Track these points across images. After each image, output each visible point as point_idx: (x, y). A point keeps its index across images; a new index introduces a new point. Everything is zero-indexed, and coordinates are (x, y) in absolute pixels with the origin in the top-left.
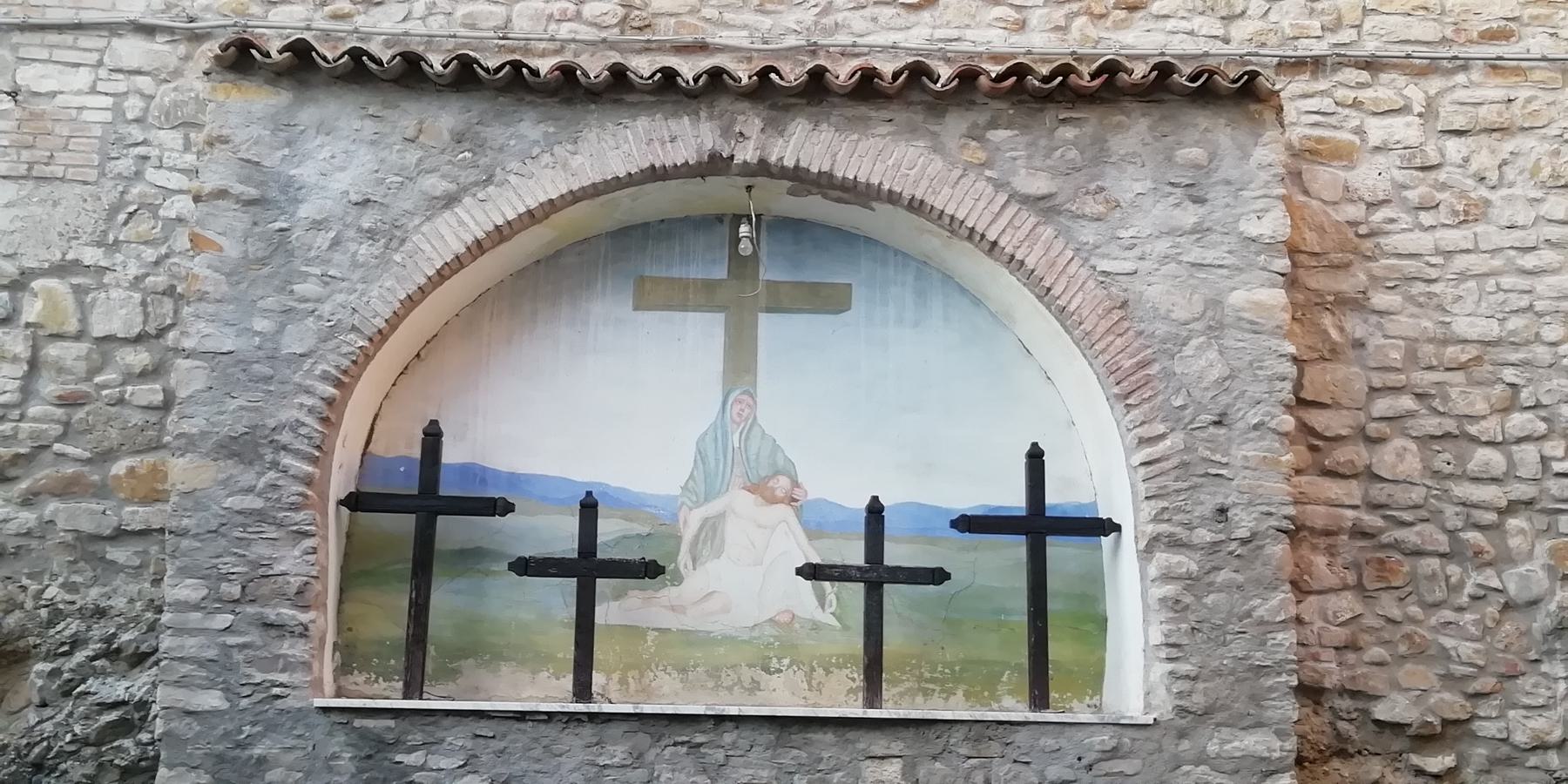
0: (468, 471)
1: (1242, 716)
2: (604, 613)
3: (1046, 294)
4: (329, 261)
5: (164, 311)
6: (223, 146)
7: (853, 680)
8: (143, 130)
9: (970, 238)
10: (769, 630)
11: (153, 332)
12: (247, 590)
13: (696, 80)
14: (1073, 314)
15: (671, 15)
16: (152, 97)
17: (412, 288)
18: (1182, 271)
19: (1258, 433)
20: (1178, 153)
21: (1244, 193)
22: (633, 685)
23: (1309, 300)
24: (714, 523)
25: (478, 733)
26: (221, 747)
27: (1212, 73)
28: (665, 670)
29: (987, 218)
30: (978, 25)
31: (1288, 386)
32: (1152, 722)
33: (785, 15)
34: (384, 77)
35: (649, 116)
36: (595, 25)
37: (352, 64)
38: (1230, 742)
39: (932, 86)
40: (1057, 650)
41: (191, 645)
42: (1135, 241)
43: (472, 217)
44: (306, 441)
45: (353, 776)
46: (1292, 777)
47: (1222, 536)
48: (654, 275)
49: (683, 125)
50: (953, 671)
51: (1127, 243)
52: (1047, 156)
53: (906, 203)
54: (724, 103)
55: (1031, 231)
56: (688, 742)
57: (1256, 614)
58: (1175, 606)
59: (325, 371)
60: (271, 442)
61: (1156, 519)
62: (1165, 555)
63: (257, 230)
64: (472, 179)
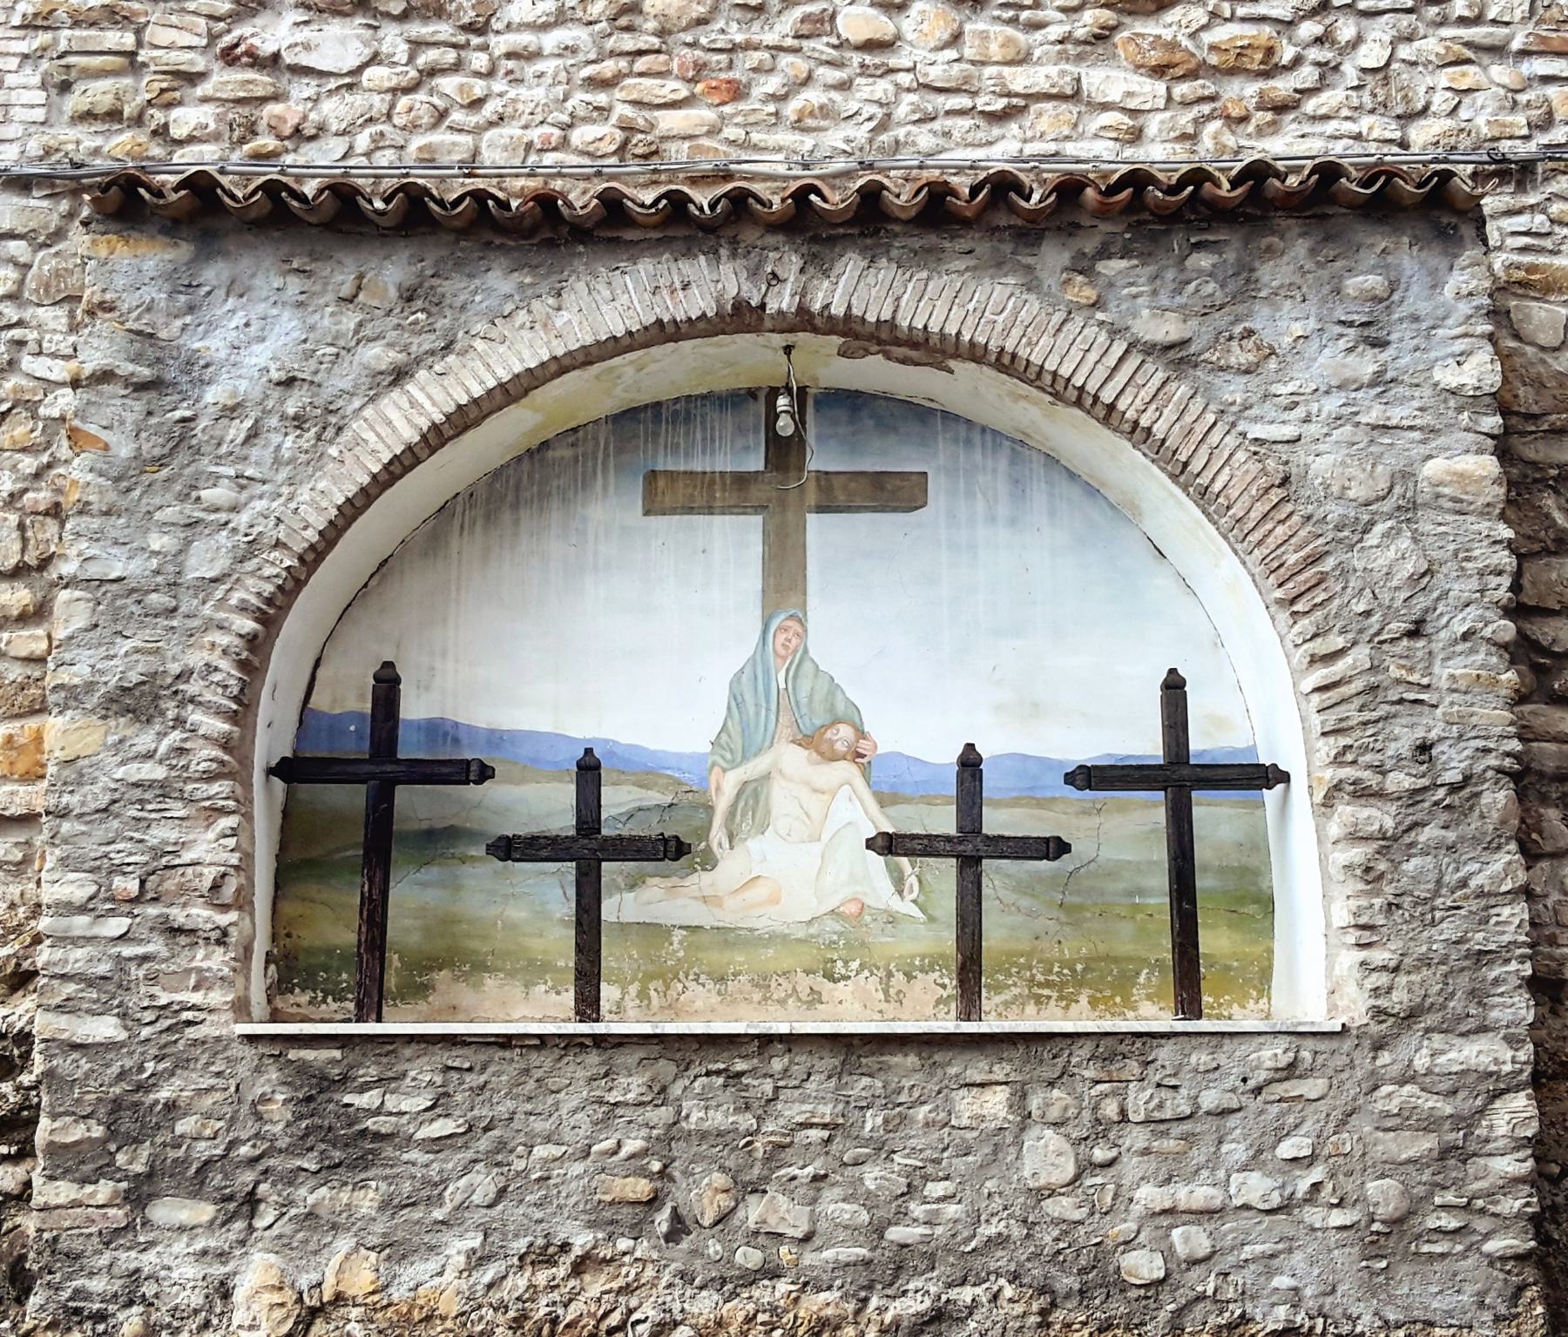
0: (435, 729)
1: (1459, 1019)
2: (616, 907)
3: (1182, 472)
4: (246, 459)
5: (48, 535)
6: (108, 316)
7: (944, 986)
8: (19, 307)
9: (1078, 403)
10: (832, 925)
11: (34, 563)
12: (149, 885)
13: (712, 206)
14: (1218, 496)
15: (684, 138)
16: (28, 266)
17: (351, 490)
18: (1362, 436)
19: (1468, 645)
20: (1349, 282)
21: (1440, 332)
22: (655, 1002)
23: (1526, 476)
24: (755, 789)
25: (450, 1063)
26: (117, 1090)
27: (1391, 175)
28: (696, 980)
29: (1101, 373)
30: (1082, 136)
31: (1506, 581)
32: (1339, 1029)
33: (830, 132)
34: (312, 219)
35: (653, 256)
36: (588, 154)
37: (269, 206)
38: (1443, 1052)
39: (1023, 203)
40: (1213, 941)
41: (77, 958)
42: (1296, 398)
43: (429, 397)
44: (220, 690)
45: (288, 1125)
46: (1529, 1097)
47: (1425, 782)
48: (670, 468)
49: (698, 268)
50: (1074, 971)
51: (1284, 401)
52: (1178, 291)
53: (993, 358)
54: (750, 235)
55: (1159, 390)
56: (726, 1070)
57: (1473, 883)
58: (1369, 875)
59: (243, 601)
60: (176, 692)
61: (1338, 760)
62: (1349, 809)
63: (153, 421)
64: (426, 347)
